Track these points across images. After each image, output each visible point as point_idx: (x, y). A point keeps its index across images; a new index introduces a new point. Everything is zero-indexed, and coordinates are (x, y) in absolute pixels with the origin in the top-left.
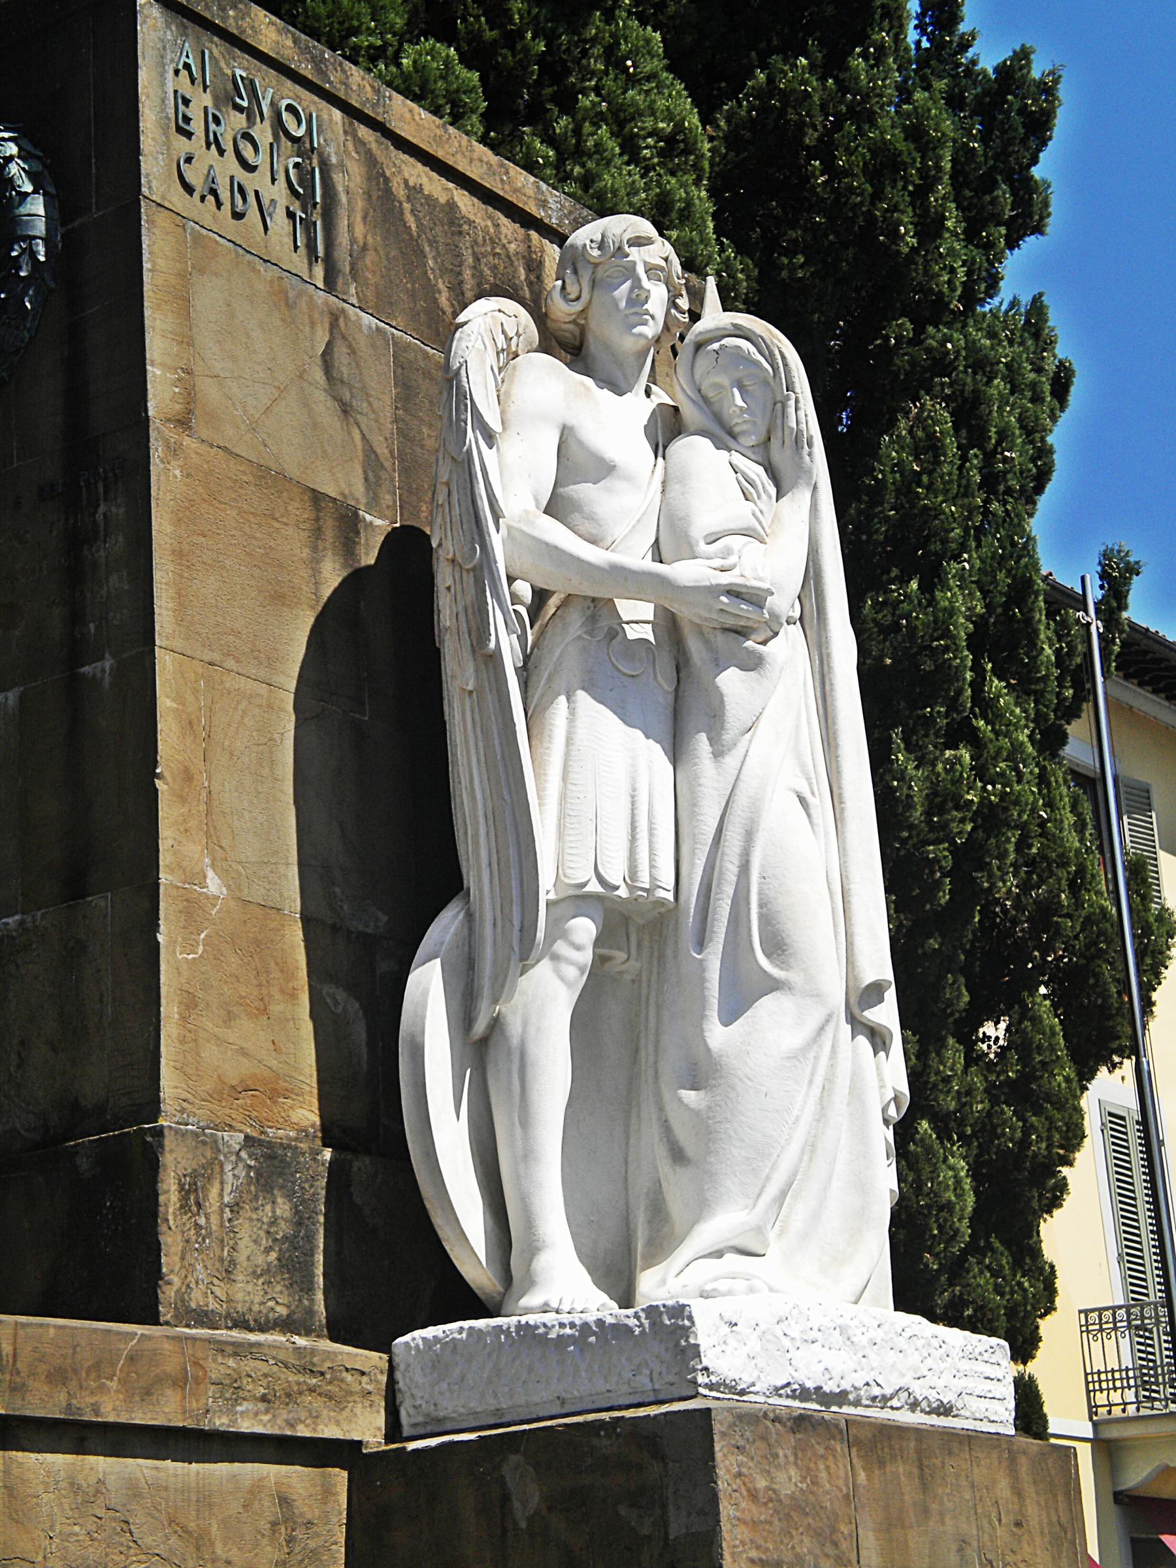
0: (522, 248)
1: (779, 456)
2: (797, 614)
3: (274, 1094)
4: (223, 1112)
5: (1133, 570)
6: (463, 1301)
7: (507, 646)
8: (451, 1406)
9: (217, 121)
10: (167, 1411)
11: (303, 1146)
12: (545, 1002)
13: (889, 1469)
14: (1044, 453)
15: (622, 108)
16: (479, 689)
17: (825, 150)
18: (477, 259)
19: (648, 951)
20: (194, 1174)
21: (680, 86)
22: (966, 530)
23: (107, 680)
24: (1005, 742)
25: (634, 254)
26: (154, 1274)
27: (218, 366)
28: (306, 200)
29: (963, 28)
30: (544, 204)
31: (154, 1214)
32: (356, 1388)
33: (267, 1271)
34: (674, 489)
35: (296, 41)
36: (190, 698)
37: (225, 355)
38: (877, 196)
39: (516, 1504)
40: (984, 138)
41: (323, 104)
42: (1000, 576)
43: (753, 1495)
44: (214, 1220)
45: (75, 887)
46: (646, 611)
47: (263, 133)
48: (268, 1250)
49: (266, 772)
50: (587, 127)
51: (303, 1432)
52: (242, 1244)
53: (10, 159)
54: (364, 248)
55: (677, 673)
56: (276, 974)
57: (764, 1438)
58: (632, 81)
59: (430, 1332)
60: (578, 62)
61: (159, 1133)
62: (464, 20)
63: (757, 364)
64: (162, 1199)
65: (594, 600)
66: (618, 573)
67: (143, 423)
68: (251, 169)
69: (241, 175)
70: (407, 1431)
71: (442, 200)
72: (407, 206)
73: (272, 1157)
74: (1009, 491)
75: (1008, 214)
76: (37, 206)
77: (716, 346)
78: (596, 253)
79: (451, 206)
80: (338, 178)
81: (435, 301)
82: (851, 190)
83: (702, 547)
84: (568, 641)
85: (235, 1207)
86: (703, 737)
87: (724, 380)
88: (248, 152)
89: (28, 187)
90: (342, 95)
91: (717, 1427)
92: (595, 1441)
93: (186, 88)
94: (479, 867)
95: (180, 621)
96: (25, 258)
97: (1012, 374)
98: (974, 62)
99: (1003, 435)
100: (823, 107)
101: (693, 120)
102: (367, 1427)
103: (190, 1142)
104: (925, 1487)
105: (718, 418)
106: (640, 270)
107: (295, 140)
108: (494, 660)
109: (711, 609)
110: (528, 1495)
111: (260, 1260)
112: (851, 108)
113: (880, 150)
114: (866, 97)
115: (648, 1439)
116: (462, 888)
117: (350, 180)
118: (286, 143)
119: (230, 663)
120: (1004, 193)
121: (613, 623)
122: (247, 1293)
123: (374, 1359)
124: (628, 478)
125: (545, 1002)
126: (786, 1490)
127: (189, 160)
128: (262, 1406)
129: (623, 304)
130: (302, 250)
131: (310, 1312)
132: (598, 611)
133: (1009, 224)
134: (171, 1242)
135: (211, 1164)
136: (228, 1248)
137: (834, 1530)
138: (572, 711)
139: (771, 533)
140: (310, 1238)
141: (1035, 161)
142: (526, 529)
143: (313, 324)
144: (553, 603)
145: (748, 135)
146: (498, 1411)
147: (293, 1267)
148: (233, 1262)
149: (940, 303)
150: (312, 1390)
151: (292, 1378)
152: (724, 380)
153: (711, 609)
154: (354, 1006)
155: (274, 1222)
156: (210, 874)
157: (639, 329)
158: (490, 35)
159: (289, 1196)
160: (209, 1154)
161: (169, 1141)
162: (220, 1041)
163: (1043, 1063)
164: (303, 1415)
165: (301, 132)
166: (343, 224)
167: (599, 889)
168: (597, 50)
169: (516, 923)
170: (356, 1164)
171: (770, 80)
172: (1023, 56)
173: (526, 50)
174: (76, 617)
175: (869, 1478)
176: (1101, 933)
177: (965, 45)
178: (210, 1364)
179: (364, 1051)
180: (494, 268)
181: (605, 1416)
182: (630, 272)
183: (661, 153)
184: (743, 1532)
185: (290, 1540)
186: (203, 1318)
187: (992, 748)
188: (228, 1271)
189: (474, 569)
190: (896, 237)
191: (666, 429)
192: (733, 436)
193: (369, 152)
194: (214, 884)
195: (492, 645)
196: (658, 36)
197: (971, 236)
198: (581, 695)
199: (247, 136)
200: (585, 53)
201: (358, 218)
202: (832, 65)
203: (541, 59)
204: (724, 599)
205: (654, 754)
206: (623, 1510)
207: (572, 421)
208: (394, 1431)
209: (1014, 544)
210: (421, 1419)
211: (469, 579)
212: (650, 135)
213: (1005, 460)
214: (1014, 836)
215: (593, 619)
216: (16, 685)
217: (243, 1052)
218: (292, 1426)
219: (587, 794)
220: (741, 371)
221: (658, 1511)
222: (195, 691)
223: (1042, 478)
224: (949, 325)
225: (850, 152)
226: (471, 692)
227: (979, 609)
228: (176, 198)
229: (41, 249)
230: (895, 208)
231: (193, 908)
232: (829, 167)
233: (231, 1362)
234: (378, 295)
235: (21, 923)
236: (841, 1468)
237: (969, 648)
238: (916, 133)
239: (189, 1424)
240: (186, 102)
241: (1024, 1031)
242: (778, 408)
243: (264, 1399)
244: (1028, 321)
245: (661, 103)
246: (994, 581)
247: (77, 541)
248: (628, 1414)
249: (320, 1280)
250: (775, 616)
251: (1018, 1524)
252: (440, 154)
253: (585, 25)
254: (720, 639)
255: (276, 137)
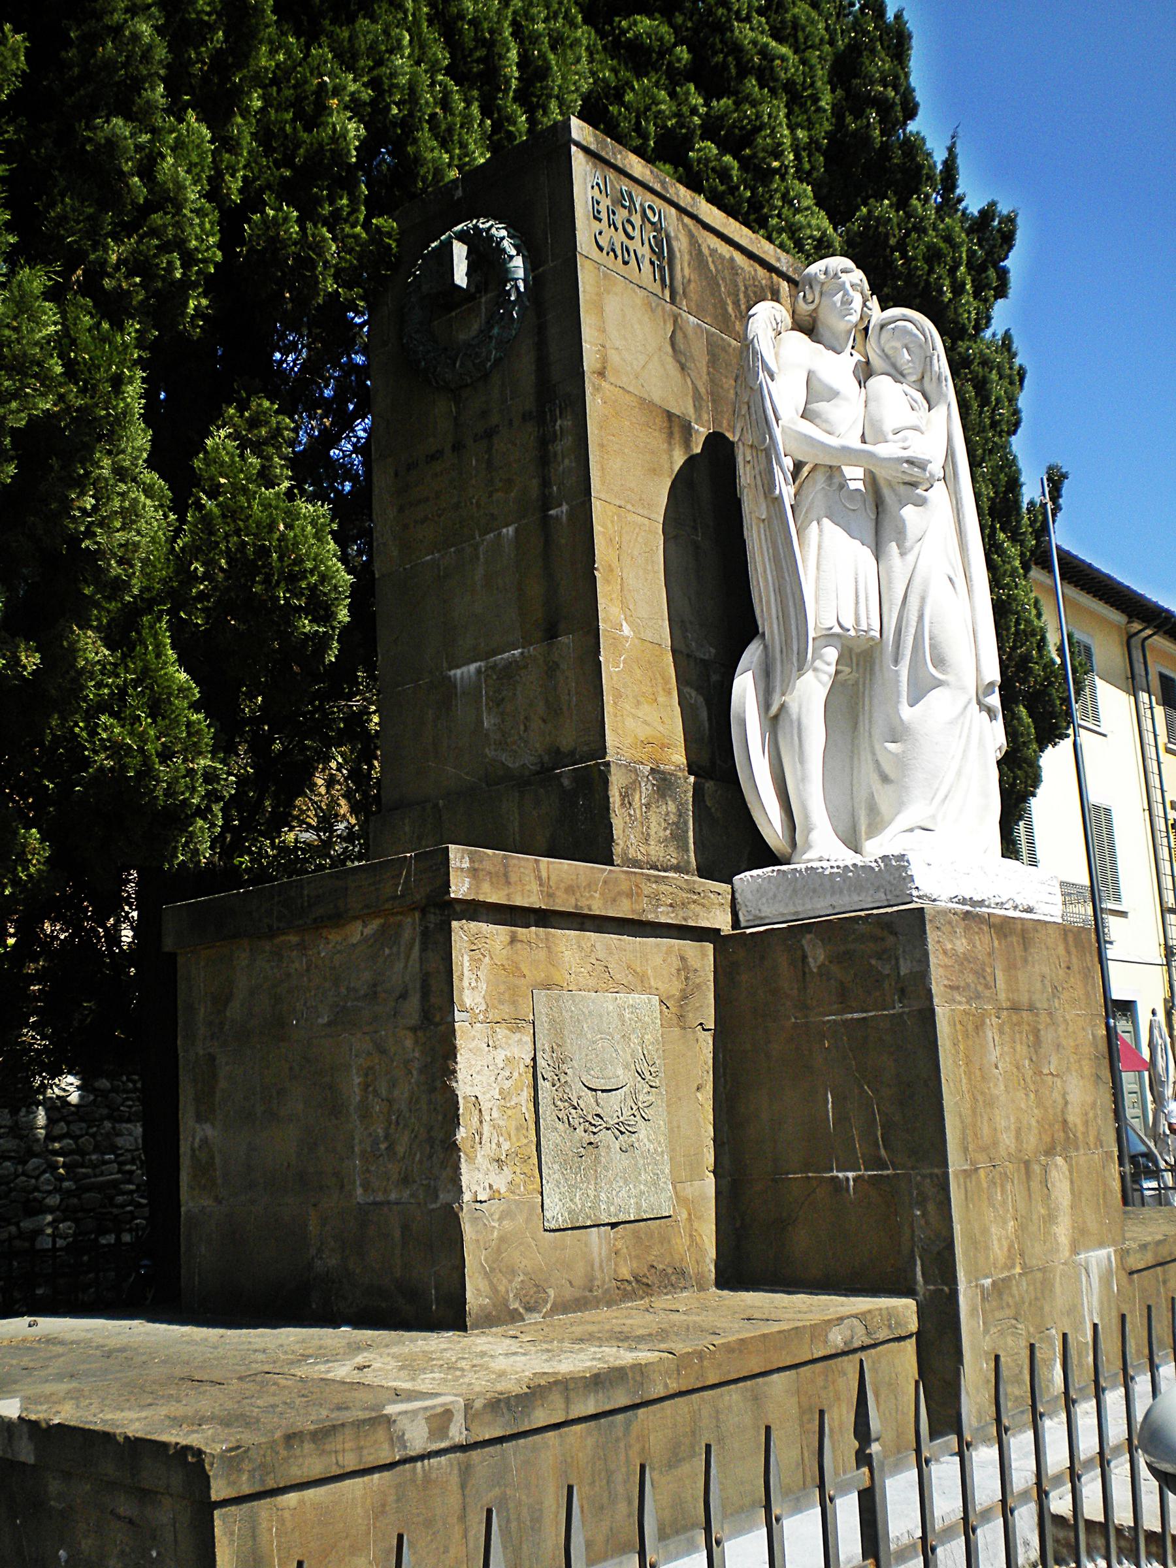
0: (769, 283)
1: (929, 386)
2: (942, 475)
3: (663, 746)
4: (638, 756)
5: (1064, 476)
6: (765, 856)
7: (787, 491)
8: (768, 911)
9: (614, 213)
10: (623, 910)
11: (680, 774)
12: (810, 693)
13: (1009, 939)
14: (1016, 412)
15: (793, 224)
16: (769, 518)
17: (902, 247)
18: (746, 288)
19: (861, 662)
20: (627, 787)
21: (823, 213)
22: (984, 450)
23: (564, 517)
24: (1008, 567)
25: (844, 277)
26: (610, 839)
27: (618, 344)
28: (660, 256)
29: (958, 191)
30: (779, 260)
31: (608, 809)
32: (716, 901)
33: (665, 840)
34: (871, 405)
35: (652, 172)
36: (610, 525)
37: (622, 338)
38: (931, 271)
39: (810, 960)
40: (979, 244)
41: (666, 205)
42: (1002, 476)
43: (945, 952)
44: (638, 811)
45: (551, 633)
46: (859, 472)
47: (637, 219)
48: (665, 829)
49: (650, 568)
50: (774, 235)
51: (691, 923)
52: (652, 826)
53: (503, 238)
54: (689, 281)
55: (877, 510)
56: (660, 680)
57: (950, 923)
58: (798, 211)
59: (755, 872)
60: (768, 201)
61: (608, 764)
62: (707, 180)
63: (915, 335)
64: (611, 800)
65: (830, 467)
66: (845, 450)
67: (582, 374)
68: (631, 238)
69: (626, 241)
70: (743, 924)
71: (728, 256)
72: (710, 259)
73: (665, 780)
74: (1002, 431)
75: (995, 285)
76: (518, 262)
77: (893, 326)
78: (823, 277)
79: (732, 259)
80: (675, 244)
81: (726, 310)
82: (917, 268)
83: (891, 437)
84: (817, 488)
85: (648, 806)
86: (894, 544)
87: (898, 345)
88: (629, 229)
89: (513, 252)
90: (675, 200)
91: (927, 917)
92: (856, 927)
93: (597, 196)
94: (771, 618)
95: (603, 483)
96: (513, 291)
97: (1000, 368)
98: (966, 208)
99: (998, 400)
100: (899, 225)
101: (830, 231)
102: (722, 921)
103: (624, 770)
104: (1025, 949)
105: (894, 366)
106: (848, 286)
107: (653, 224)
108: (779, 500)
109: (897, 471)
110: (817, 956)
111: (661, 834)
112: (914, 226)
113: (931, 247)
114: (922, 220)
115: (887, 924)
116: (757, 632)
117: (681, 245)
118: (648, 226)
119: (629, 507)
120: (991, 273)
121: (841, 479)
122: (656, 851)
123: (724, 888)
124: (846, 399)
125: (810, 693)
126: (961, 950)
127: (600, 233)
128: (670, 909)
129: (839, 304)
130: (658, 281)
131: (688, 862)
132: (833, 471)
133: (995, 289)
134: (618, 822)
135: (634, 782)
136: (644, 825)
137: (984, 970)
138: (821, 531)
139: (928, 429)
140: (686, 823)
141: (1006, 257)
142: (793, 427)
143: (665, 322)
144: (805, 471)
145: (858, 240)
146: (796, 913)
147: (678, 837)
148: (648, 834)
149: (963, 329)
150: (694, 902)
151: (684, 895)
152: (898, 345)
153: (897, 471)
154: (701, 699)
155: (667, 814)
156: (624, 624)
157: (847, 318)
158: (721, 188)
159: (674, 800)
160: (633, 777)
161: (613, 769)
162: (634, 716)
163: (1024, 743)
164: (691, 914)
165: (656, 219)
166: (678, 268)
167: (837, 630)
168: (778, 195)
169: (795, 648)
170: (707, 785)
171: (869, 212)
172: (993, 204)
173: (741, 196)
174: (545, 483)
175: (1000, 944)
176: (1052, 672)
177: (960, 200)
178: (643, 886)
179: (706, 724)
180: (755, 293)
181: (862, 913)
182: (842, 287)
183: (815, 248)
184: (941, 971)
185: (687, 978)
186: (636, 863)
187: (1002, 570)
188: (647, 840)
189: (765, 449)
190: (941, 293)
191: (865, 373)
192: (903, 376)
193: (690, 231)
194: (627, 630)
195: (777, 492)
196: (809, 188)
197: (976, 295)
198: (826, 521)
199: (629, 221)
200: (771, 197)
201: (686, 265)
202: (902, 204)
203: (749, 200)
204: (905, 465)
205: (866, 554)
206: (873, 962)
207: (813, 368)
208: (736, 924)
209: (1007, 459)
210: (751, 918)
211: (762, 455)
212: (809, 238)
213: (1000, 414)
214: (1014, 618)
215: (830, 477)
216: (513, 523)
217: (645, 722)
218: (685, 920)
219: (830, 576)
220: (907, 340)
221: (893, 962)
222: (612, 522)
223: (1017, 424)
224: (969, 340)
225: (915, 248)
226: (763, 520)
227: (992, 494)
228: (595, 253)
229: (521, 285)
230: (940, 278)
231: (617, 641)
232: (904, 255)
233: (654, 886)
234: (697, 306)
235: (522, 653)
236: (987, 939)
237: (989, 514)
238: (948, 239)
239: (636, 917)
240: (598, 203)
241: (1014, 726)
242: (928, 360)
243: (671, 905)
244: (1003, 343)
245: (814, 222)
246: (999, 479)
247: (544, 442)
248: (875, 912)
249: (692, 846)
250: (932, 475)
251: (1069, 968)
252: (726, 232)
253: (771, 182)
254: (902, 489)
255: (643, 221)
